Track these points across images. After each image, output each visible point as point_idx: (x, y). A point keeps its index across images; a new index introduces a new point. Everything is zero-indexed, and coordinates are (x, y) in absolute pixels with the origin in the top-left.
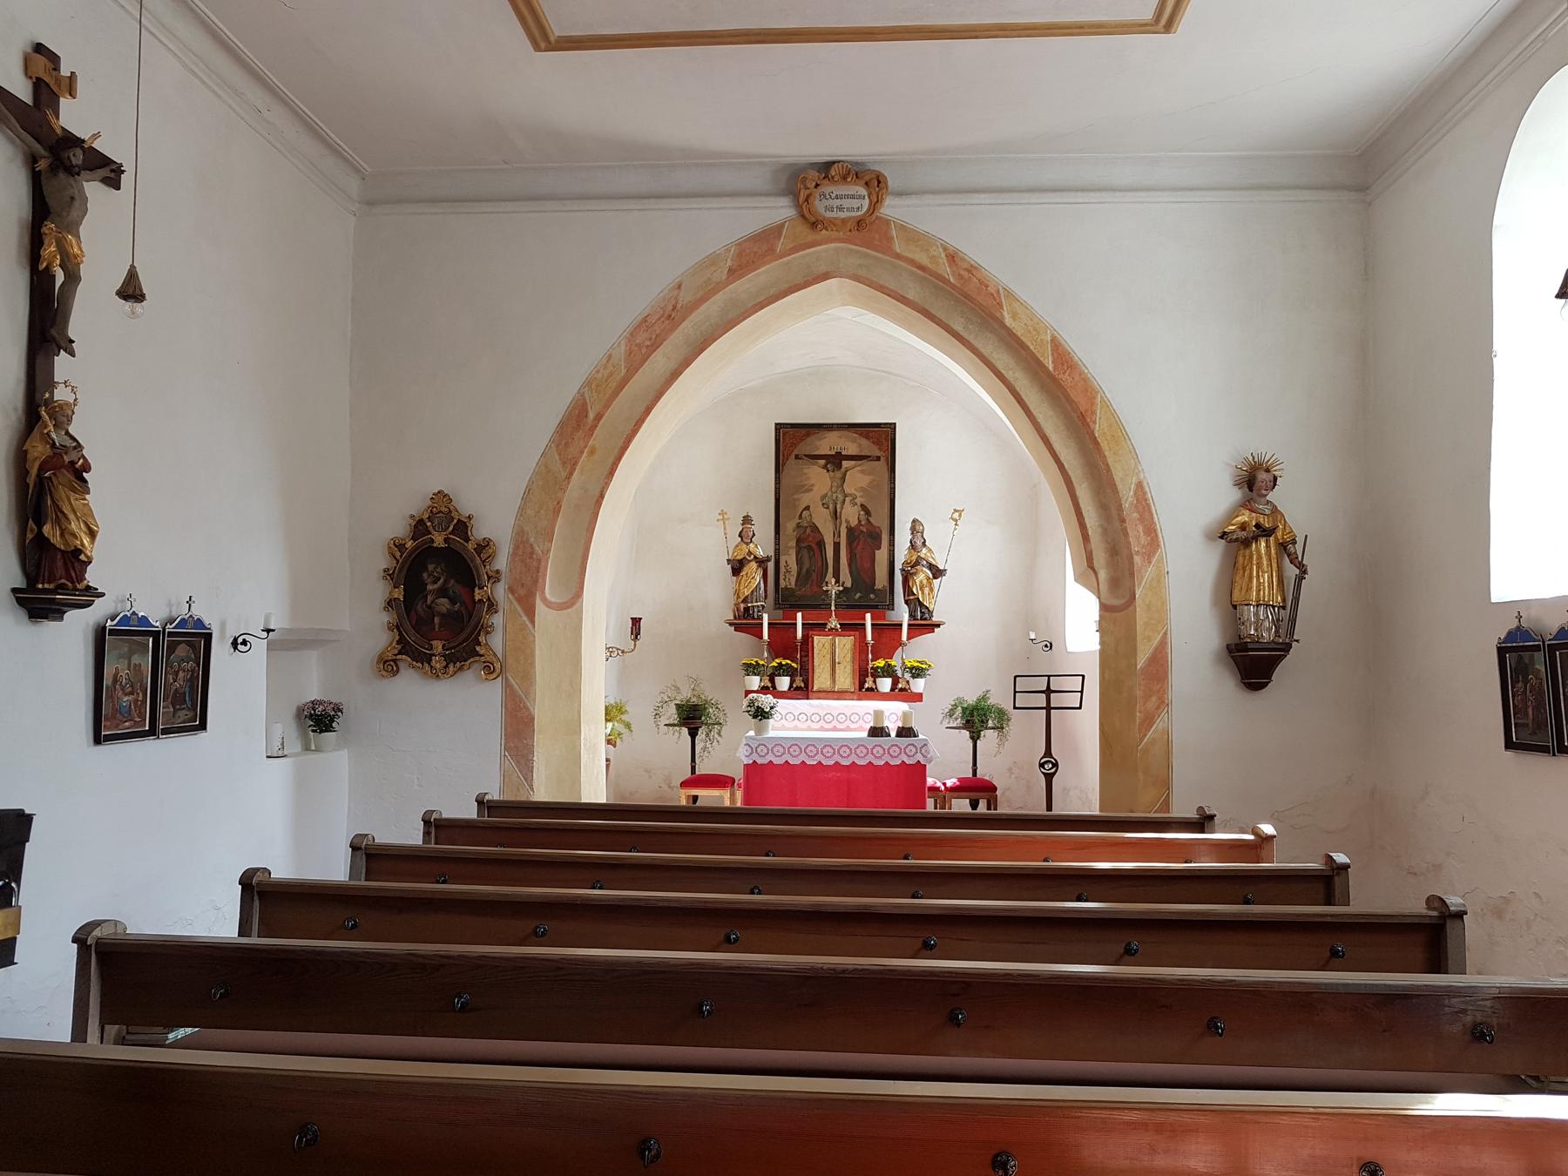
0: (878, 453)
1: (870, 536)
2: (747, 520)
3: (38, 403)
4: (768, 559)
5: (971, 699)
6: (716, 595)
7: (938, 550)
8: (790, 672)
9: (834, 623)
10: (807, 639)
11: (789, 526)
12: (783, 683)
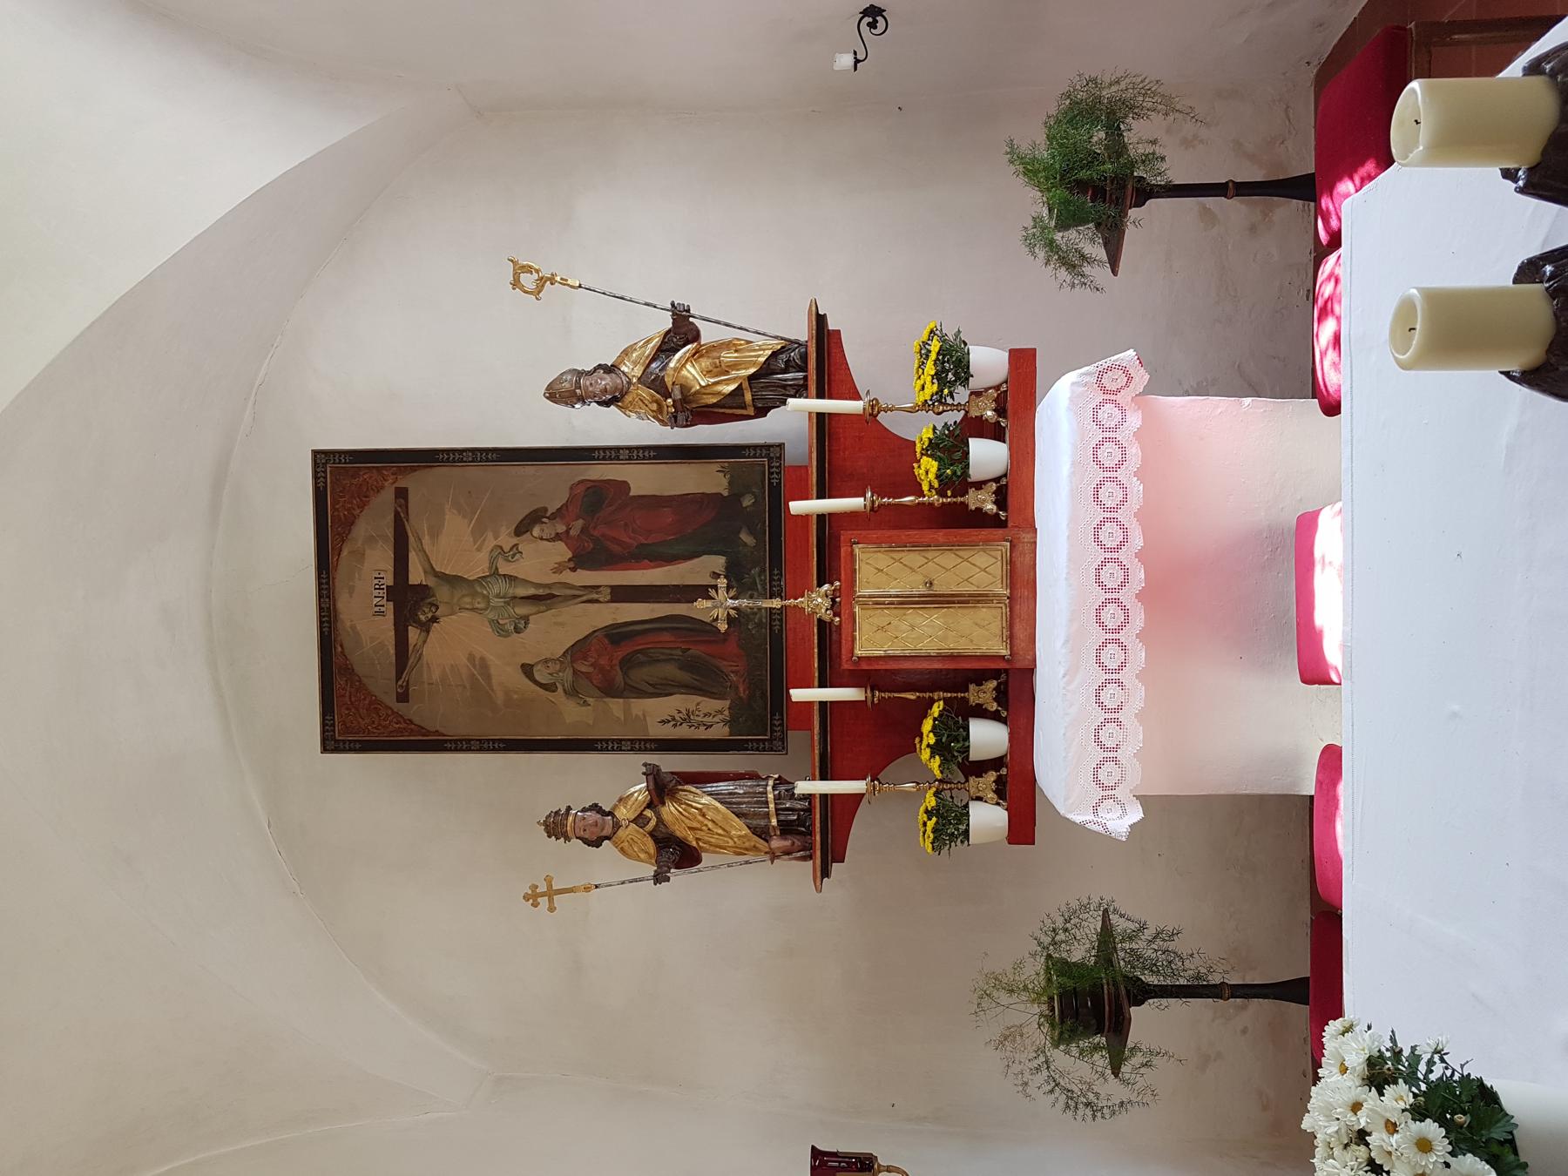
0: (388, 495)
1: (594, 509)
2: (556, 827)
3: (911, 411)
4: (653, 774)
5: (1031, 203)
6: (748, 894)
7: (618, 333)
8: (960, 715)
9: (817, 601)
10: (863, 675)
11: (575, 716)
12: (987, 737)
